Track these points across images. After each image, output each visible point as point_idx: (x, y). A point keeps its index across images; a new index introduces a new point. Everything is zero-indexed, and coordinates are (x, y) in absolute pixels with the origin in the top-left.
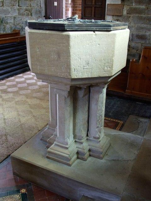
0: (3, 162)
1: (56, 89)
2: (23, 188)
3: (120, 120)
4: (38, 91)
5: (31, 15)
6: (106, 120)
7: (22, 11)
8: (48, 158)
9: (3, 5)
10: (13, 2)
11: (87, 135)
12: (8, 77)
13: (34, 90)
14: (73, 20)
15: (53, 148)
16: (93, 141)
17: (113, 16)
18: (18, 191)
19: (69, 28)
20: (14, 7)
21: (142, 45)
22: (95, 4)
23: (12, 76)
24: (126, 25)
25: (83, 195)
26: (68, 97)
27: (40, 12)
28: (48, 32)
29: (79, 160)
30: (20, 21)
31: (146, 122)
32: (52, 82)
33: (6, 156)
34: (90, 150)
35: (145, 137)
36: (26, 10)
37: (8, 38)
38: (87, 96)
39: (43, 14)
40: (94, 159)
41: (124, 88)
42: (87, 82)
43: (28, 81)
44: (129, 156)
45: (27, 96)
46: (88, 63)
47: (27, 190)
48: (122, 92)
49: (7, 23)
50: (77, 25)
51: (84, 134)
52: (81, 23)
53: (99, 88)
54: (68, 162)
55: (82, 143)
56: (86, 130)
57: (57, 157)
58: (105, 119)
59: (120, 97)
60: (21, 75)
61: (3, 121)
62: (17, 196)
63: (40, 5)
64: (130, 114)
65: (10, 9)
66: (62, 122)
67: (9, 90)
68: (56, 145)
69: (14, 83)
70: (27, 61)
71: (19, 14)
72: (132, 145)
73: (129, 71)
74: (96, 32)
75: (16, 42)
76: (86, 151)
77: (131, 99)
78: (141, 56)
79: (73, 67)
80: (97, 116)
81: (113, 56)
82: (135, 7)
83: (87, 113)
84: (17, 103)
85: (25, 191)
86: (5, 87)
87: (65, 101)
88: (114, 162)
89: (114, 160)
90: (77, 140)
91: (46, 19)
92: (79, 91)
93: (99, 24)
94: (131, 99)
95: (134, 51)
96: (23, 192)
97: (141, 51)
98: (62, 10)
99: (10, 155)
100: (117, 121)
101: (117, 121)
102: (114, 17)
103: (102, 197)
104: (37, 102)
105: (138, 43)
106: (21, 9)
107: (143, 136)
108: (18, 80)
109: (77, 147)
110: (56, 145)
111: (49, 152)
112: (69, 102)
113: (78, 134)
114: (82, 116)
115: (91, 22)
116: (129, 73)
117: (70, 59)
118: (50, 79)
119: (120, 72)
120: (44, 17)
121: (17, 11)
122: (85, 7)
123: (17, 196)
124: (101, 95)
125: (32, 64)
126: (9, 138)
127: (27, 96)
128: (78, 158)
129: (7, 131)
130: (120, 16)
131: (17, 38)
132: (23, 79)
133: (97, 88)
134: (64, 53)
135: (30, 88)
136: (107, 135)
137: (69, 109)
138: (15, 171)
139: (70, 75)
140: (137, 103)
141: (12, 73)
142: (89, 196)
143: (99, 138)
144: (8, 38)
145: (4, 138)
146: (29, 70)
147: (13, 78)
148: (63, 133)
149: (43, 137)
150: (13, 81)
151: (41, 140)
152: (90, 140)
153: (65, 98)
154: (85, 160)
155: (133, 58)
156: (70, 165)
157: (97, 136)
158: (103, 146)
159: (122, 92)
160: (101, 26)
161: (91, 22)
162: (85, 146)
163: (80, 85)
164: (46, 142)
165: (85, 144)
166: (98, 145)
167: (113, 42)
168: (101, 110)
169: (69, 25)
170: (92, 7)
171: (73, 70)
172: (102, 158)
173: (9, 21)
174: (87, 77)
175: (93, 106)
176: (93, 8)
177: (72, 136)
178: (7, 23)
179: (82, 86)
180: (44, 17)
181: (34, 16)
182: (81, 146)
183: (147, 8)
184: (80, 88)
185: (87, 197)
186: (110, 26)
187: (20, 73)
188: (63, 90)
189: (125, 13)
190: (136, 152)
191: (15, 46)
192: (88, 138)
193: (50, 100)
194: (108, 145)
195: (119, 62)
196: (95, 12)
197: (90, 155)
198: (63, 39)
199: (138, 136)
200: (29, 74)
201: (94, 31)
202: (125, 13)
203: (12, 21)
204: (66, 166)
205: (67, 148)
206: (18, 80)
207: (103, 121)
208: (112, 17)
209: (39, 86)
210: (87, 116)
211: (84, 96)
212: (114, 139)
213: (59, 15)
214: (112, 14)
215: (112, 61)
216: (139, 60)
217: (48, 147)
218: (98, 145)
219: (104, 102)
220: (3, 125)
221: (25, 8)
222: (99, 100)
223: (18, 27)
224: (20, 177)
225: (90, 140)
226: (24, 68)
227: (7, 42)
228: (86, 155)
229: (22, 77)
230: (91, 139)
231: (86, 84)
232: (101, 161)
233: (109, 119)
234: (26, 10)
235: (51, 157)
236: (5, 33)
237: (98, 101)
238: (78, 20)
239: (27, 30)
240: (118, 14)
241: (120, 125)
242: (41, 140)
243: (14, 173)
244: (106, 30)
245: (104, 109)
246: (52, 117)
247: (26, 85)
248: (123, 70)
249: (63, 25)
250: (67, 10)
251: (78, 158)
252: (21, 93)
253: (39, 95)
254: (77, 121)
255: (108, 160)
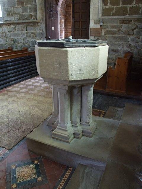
0: (20, 142)
1: (58, 88)
2: (36, 160)
3: (103, 110)
4: (42, 91)
5: (36, 36)
6: (94, 110)
7: (29, 34)
8: (53, 138)
9: (15, 30)
10: (22, 28)
11: (81, 121)
12: (20, 82)
13: (40, 90)
14: (69, 40)
15: (57, 131)
16: (85, 125)
17: (95, 36)
18: (32, 162)
19: (67, 46)
20: (23, 31)
21: (116, 57)
22: (82, 28)
23: (23, 81)
24: (106, 42)
25: (79, 163)
26: (67, 94)
27: (42, 34)
28: (52, 48)
29: (75, 139)
30: (28, 41)
31: (121, 111)
32: (55, 84)
33: (22, 138)
34: (83, 132)
35: (121, 121)
36: (32, 33)
37: (19, 54)
38: (80, 93)
39: (45, 36)
40: (86, 138)
41: (104, 87)
42: (80, 83)
43: (35, 84)
44: (111, 135)
45: (35, 95)
46: (81, 69)
47: (39, 162)
48: (103, 90)
49: (18, 43)
50: (73, 43)
51: (78, 120)
52: (75, 42)
53: (65, 93)
54: (67, 141)
55: (77, 127)
56: (80, 117)
57: (60, 137)
58: (93, 110)
59: (102, 94)
60: (29, 80)
61: (18, 113)
62: (32, 166)
63: (42, 30)
64: (109, 106)
65: (20, 33)
66: (63, 112)
67: (22, 91)
68: (58, 128)
69: (25, 86)
70: (36, 69)
71: (27, 36)
72: (112, 127)
73: (108, 75)
74: (86, 48)
75: (25, 56)
76: (80, 132)
77: (109, 95)
78: (116, 64)
79: (70, 72)
80: (87, 107)
81: (98, 64)
82: (109, 30)
83: (80, 105)
84: (28, 100)
85: (37, 162)
86: (18, 89)
87: (65, 97)
88: (100, 139)
89: (99, 138)
90: (73, 125)
91: (47, 39)
92: (75, 90)
93: (88, 42)
94: (109, 95)
95: (111, 61)
96: (36, 163)
97: (116, 61)
98: (58, 33)
99: (25, 137)
100: (100, 111)
101: (100, 111)
102: (96, 37)
103: (93, 164)
104: (42, 99)
105: (113, 55)
106: (28, 32)
107: (120, 120)
108: (27, 83)
109: (73, 130)
110: (58, 128)
111: (54, 134)
112: (67, 97)
113: (74, 121)
114: (76, 107)
115: (82, 41)
116: (108, 77)
117: (68, 67)
118: (53, 81)
119: (103, 75)
120: (45, 38)
121: (26, 34)
122: (74, 30)
123: (32, 166)
124: (90, 92)
125: (41, 71)
126: (23, 125)
127: (35, 95)
128: (74, 137)
129: (22, 120)
130: (100, 36)
131: (26, 53)
132: (31, 83)
133: (86, 87)
134: (64, 63)
135: (36, 89)
136: (94, 121)
137: (67, 103)
138: (30, 148)
139: (68, 78)
140: (114, 97)
141: (25, 78)
142: (84, 164)
143: (89, 123)
144: (19, 54)
145: (20, 125)
146: (37, 75)
147: (23, 82)
148: (63, 120)
149: (48, 124)
150: (24, 84)
151: (47, 125)
152: (83, 124)
153: (65, 94)
154: (79, 138)
155: (110, 66)
156: (69, 143)
157: (88, 121)
158: (92, 128)
159: (103, 90)
160: (89, 43)
161: (82, 41)
162: (80, 128)
163: (75, 85)
164: (51, 126)
165: (80, 127)
166: (88, 128)
167: (98, 55)
168: (90, 102)
169: (67, 44)
170: (79, 30)
171: (70, 75)
172: (91, 137)
173: (20, 42)
174: (80, 79)
175: (84, 100)
176: (80, 31)
177: (69, 122)
178: (18, 43)
179: (76, 86)
180: (45, 38)
181: (37, 38)
182: (76, 129)
183: (119, 31)
184: (75, 88)
185: (82, 164)
186: (95, 43)
187: (29, 79)
188: (63, 89)
189: (103, 34)
190: (116, 132)
191: (25, 59)
192: (81, 123)
193: (53, 97)
194: (96, 127)
195: (102, 69)
196: (81, 34)
197: (83, 135)
198: (63, 53)
199: (116, 120)
200: (34, 79)
201: (84, 47)
202: (103, 34)
203: (22, 41)
204: (66, 143)
205: (66, 131)
206: (27, 83)
207: (92, 111)
208: (94, 37)
209: (43, 87)
210: (80, 107)
211: (78, 93)
212: (99, 123)
213: (56, 37)
214: (94, 35)
215: (98, 68)
216: (115, 67)
217: (52, 131)
218: (88, 128)
219: (92, 97)
220: (19, 116)
221: (31, 32)
222: (88, 95)
223: (26, 45)
224: (33, 152)
225: (83, 124)
226: (33, 73)
227: (19, 56)
228: (80, 135)
229: (30, 81)
230: (83, 123)
231: (79, 84)
232: (91, 139)
233: (95, 110)
234: (32, 33)
235: (55, 137)
236: (17, 50)
237: (88, 96)
238: (72, 40)
239: (37, 47)
240: (98, 35)
241: (102, 114)
242: (47, 125)
243: (29, 150)
244: (92, 46)
245: (92, 102)
246: (55, 109)
247: (33, 87)
248: (105, 74)
249: (62, 44)
250: (61, 33)
251: (74, 137)
252: (30, 93)
253: (43, 93)
254: (73, 111)
255: (96, 138)
